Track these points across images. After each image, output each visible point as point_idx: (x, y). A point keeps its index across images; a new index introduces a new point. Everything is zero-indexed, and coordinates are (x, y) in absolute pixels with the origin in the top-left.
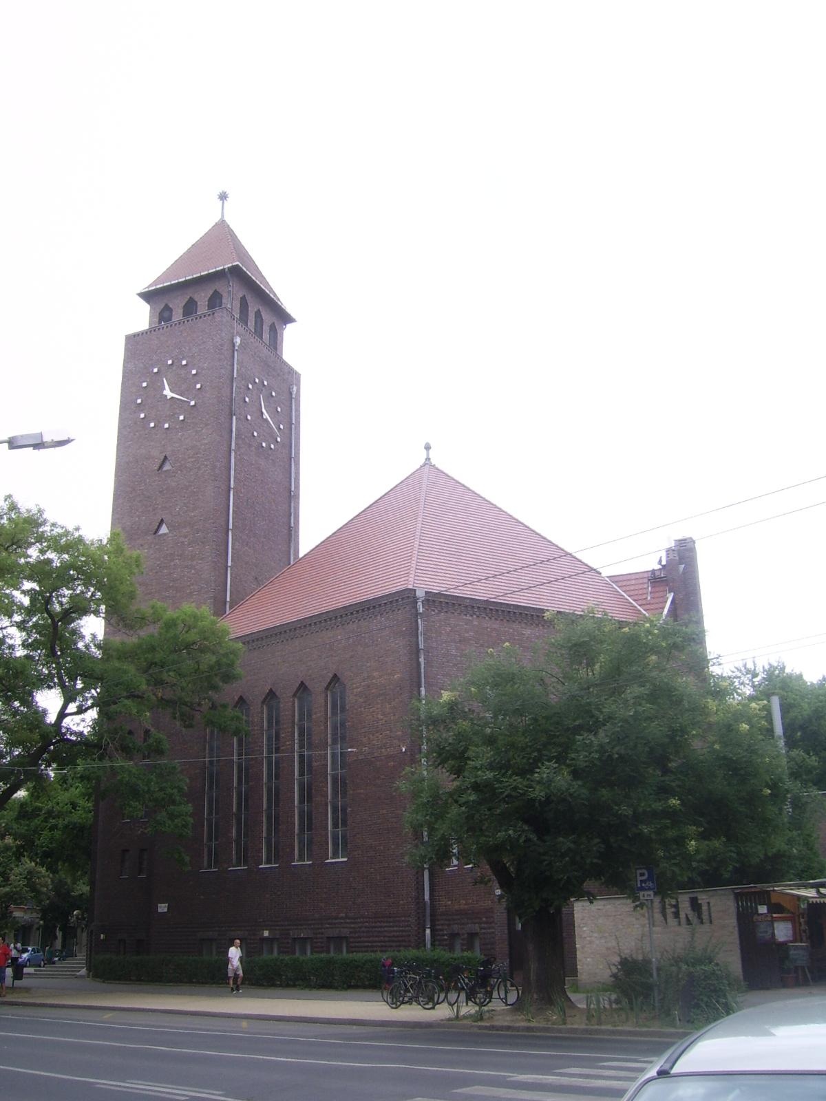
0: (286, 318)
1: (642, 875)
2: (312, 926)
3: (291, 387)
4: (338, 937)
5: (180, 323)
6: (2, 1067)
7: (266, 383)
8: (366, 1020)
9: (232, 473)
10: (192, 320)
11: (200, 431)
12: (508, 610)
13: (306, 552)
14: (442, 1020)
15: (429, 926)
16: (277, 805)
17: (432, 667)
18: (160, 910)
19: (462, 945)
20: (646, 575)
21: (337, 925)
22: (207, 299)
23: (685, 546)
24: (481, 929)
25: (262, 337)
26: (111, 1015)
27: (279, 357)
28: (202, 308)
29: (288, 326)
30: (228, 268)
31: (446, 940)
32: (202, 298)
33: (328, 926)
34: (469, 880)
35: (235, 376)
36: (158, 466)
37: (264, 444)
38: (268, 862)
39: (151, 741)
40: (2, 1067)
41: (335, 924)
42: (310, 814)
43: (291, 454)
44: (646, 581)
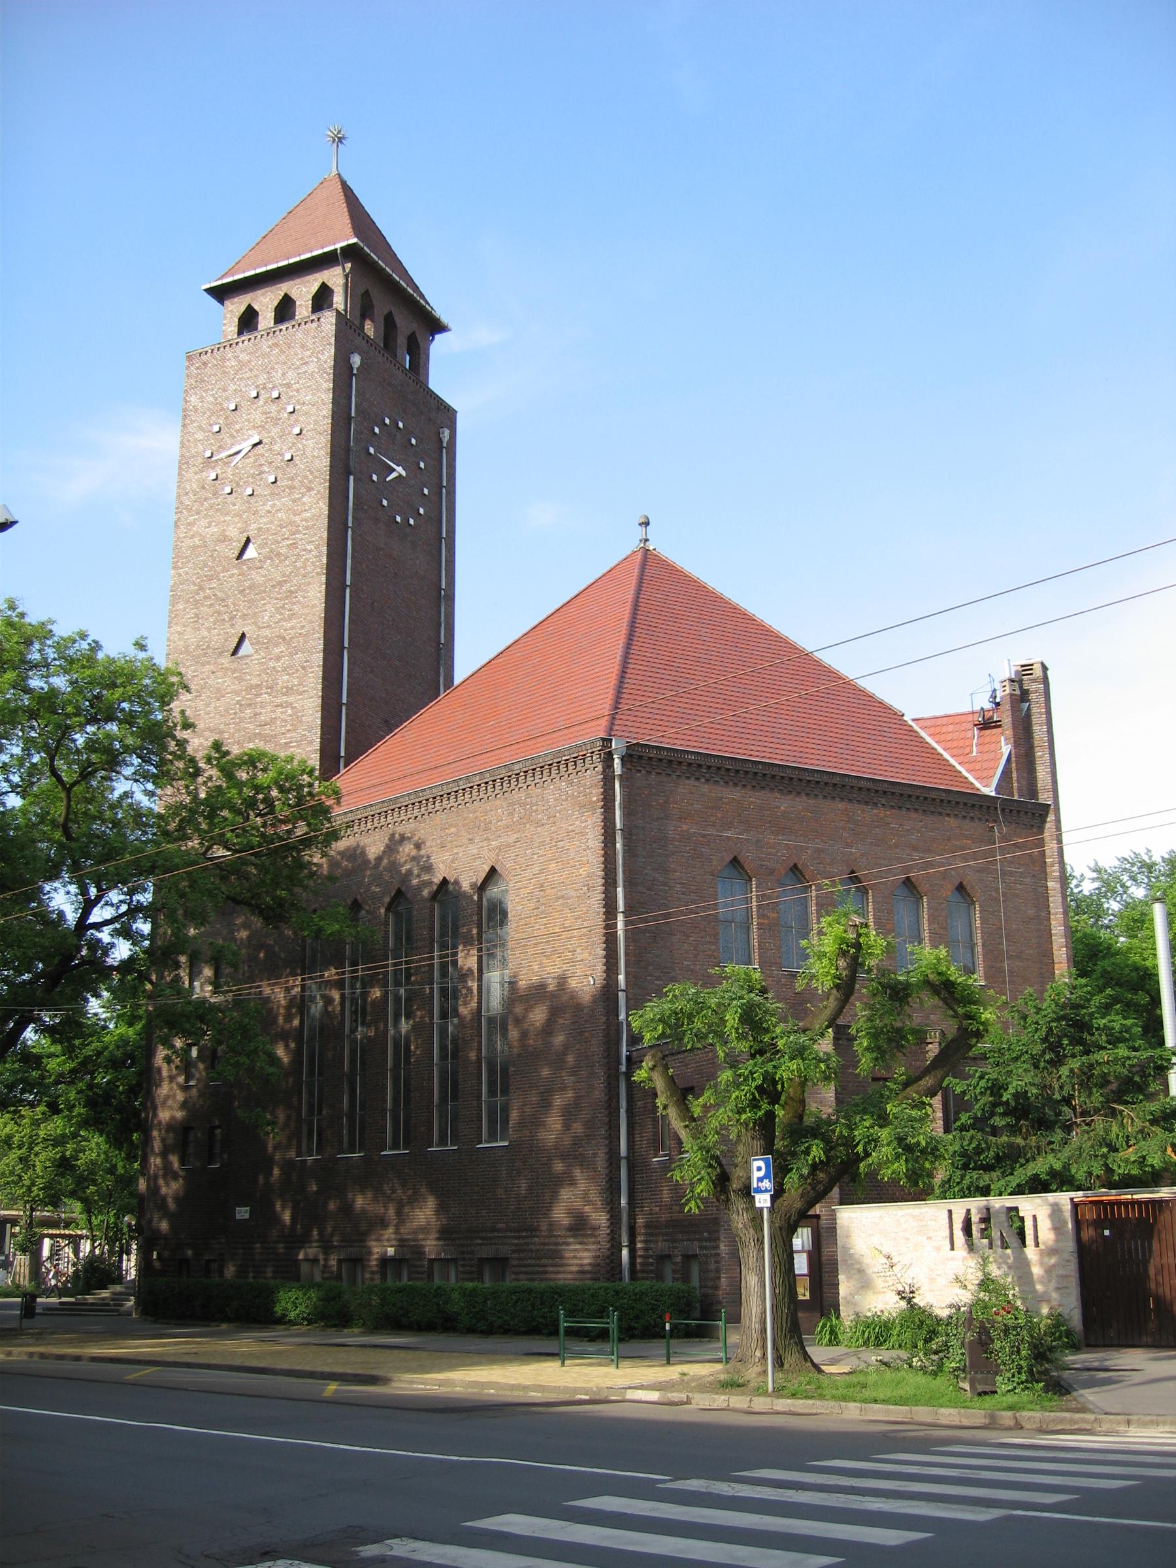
0: (436, 327)
1: (759, 1169)
2: (457, 1242)
3: (441, 430)
4: (493, 1259)
5: (268, 333)
6: (3, 1212)
7: (401, 425)
8: (328, 584)
9: (349, 562)
10: (249, 339)
11: (299, 499)
12: (782, 774)
13: (461, 680)
14: (1089, 1500)
15: (621, 910)
16: (455, 1097)
17: (637, 856)
18: (238, 1217)
19: (674, 1271)
20: (970, 718)
21: (493, 1241)
22: (310, 297)
23: (1031, 674)
24: (701, 1248)
25: (396, 355)
26: (130, 1377)
27: (422, 384)
28: (266, 319)
29: (437, 337)
30: (341, 248)
31: (652, 1264)
32: (265, 301)
33: (480, 1242)
34: (595, 799)
35: (353, 415)
36: (236, 553)
37: (398, 519)
38: (395, 1146)
39: (170, 962)
40: (3, 1212)
41: (490, 1238)
42: (455, 1073)
43: (441, 533)
44: (970, 725)
